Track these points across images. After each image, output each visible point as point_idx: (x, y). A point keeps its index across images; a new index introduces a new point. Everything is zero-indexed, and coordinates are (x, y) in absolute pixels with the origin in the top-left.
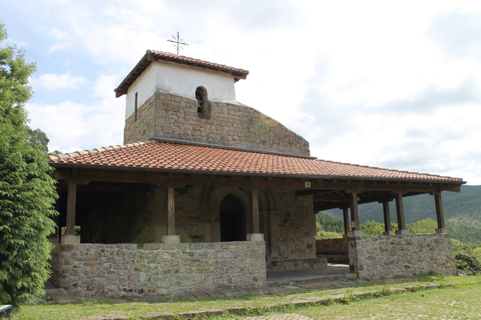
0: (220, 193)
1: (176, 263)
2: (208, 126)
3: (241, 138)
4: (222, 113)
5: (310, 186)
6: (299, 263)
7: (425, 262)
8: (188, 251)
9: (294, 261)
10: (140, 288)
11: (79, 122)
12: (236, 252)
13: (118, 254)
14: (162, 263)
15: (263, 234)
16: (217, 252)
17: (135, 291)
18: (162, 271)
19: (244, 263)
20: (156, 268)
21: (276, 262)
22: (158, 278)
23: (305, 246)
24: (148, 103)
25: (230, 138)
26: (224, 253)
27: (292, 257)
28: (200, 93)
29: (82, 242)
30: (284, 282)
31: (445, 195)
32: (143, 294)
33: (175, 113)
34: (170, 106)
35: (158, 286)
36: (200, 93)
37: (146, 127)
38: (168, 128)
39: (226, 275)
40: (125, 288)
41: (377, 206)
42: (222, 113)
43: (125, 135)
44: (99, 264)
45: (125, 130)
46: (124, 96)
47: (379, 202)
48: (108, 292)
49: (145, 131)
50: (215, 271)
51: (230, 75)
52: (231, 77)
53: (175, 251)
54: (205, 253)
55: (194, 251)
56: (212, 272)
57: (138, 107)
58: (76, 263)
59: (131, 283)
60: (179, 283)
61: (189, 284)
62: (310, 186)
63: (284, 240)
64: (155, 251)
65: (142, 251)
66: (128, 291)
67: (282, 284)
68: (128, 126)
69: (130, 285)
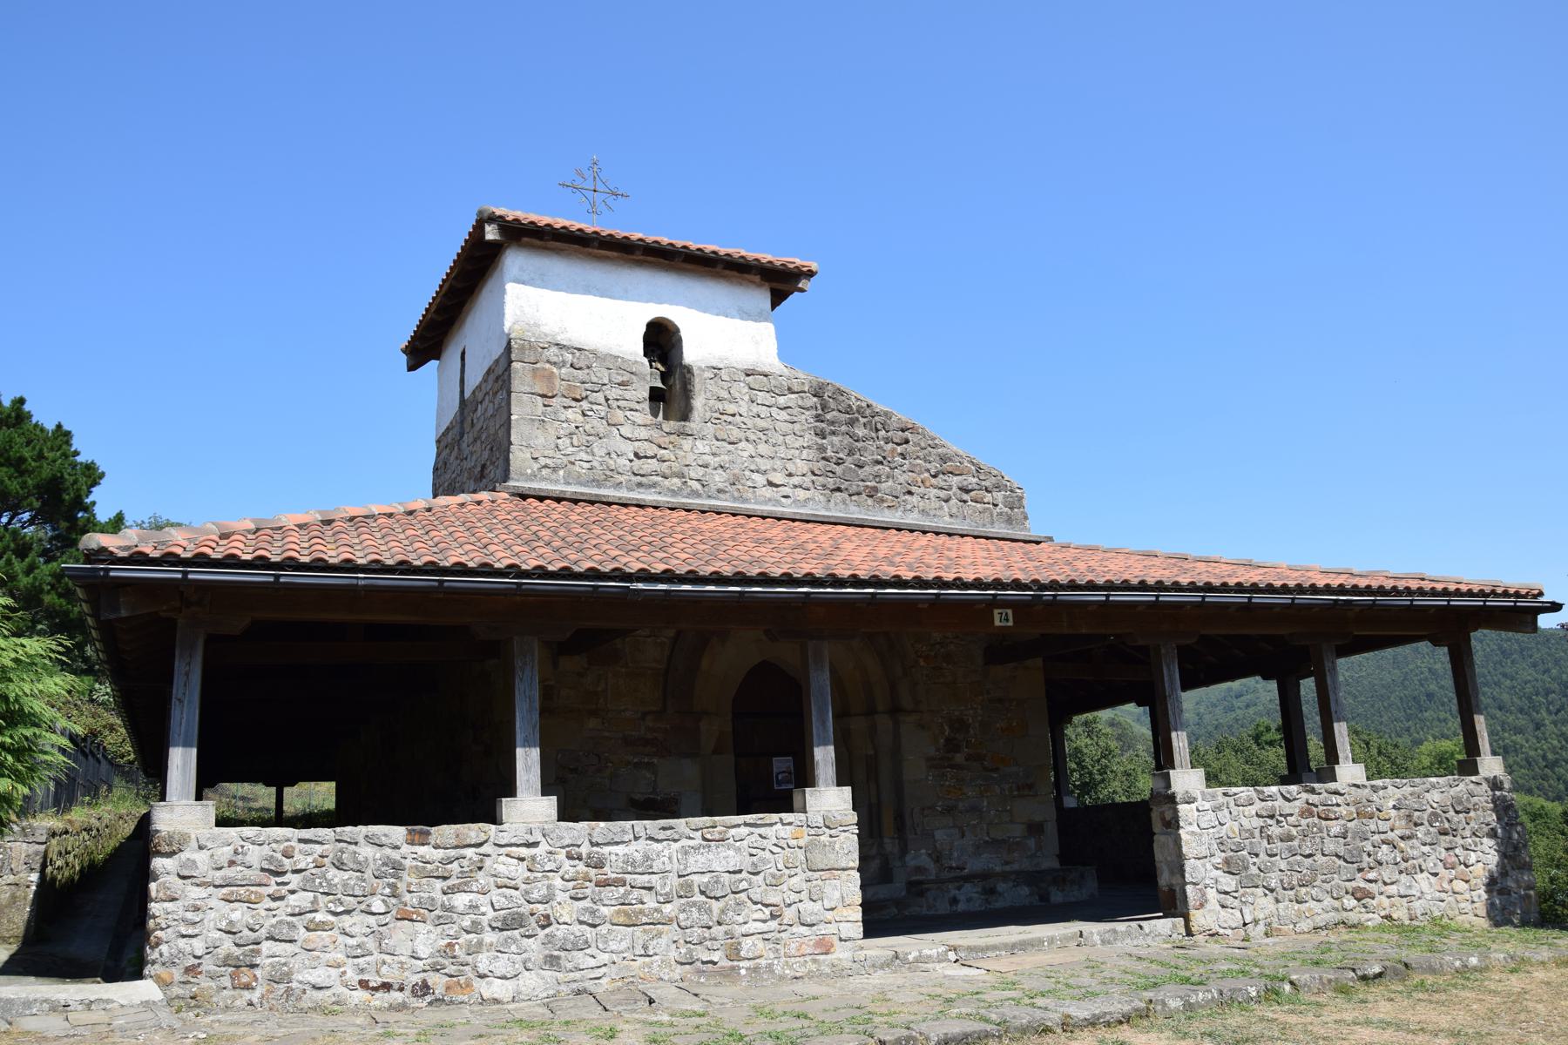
0: (732, 658)
1: (544, 891)
3: (796, 480)
5: (1010, 624)
6: (1001, 887)
7: (1425, 874)
9: (985, 876)
10: (417, 979)
12: (754, 851)
13: (339, 866)
14: (495, 891)
15: (848, 789)
16: (686, 853)
17: (401, 989)
18: (496, 919)
19: (784, 887)
20: (474, 907)
21: (920, 883)
22: (480, 943)
23: (1017, 831)
24: (492, 377)
25: (760, 479)
26: (711, 856)
27: (975, 865)
28: (661, 340)
29: (562, 817)
30: (927, 952)
31: (1483, 642)
32: (429, 998)
33: (574, 404)
34: (557, 382)
35: (481, 971)
36: (661, 340)
37: (486, 454)
38: (551, 453)
39: (718, 931)
40: (366, 977)
41: (1260, 693)
43: (434, 485)
44: (275, 899)
45: (436, 469)
46: (433, 364)
47: (1265, 678)
48: (304, 991)
49: (484, 467)
50: (682, 916)
51: (757, 278)
52: (759, 286)
54: (647, 858)
56: (671, 920)
57: (467, 395)
58: (195, 893)
59: (384, 963)
60: (552, 961)
61: (593, 963)
62: (1010, 624)
63: (949, 810)
65: (422, 850)
66: (376, 989)
67: (917, 960)
68: (444, 454)
69: (384, 969)
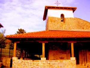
2: (65, 25)
4: (69, 21)
8: (49, 62)
11: (10, 31)
28: (62, 15)
36: (62, 15)
42: (69, 21)
53: (44, 62)
55: (50, 63)
64: (38, 62)
65: (34, 62)
